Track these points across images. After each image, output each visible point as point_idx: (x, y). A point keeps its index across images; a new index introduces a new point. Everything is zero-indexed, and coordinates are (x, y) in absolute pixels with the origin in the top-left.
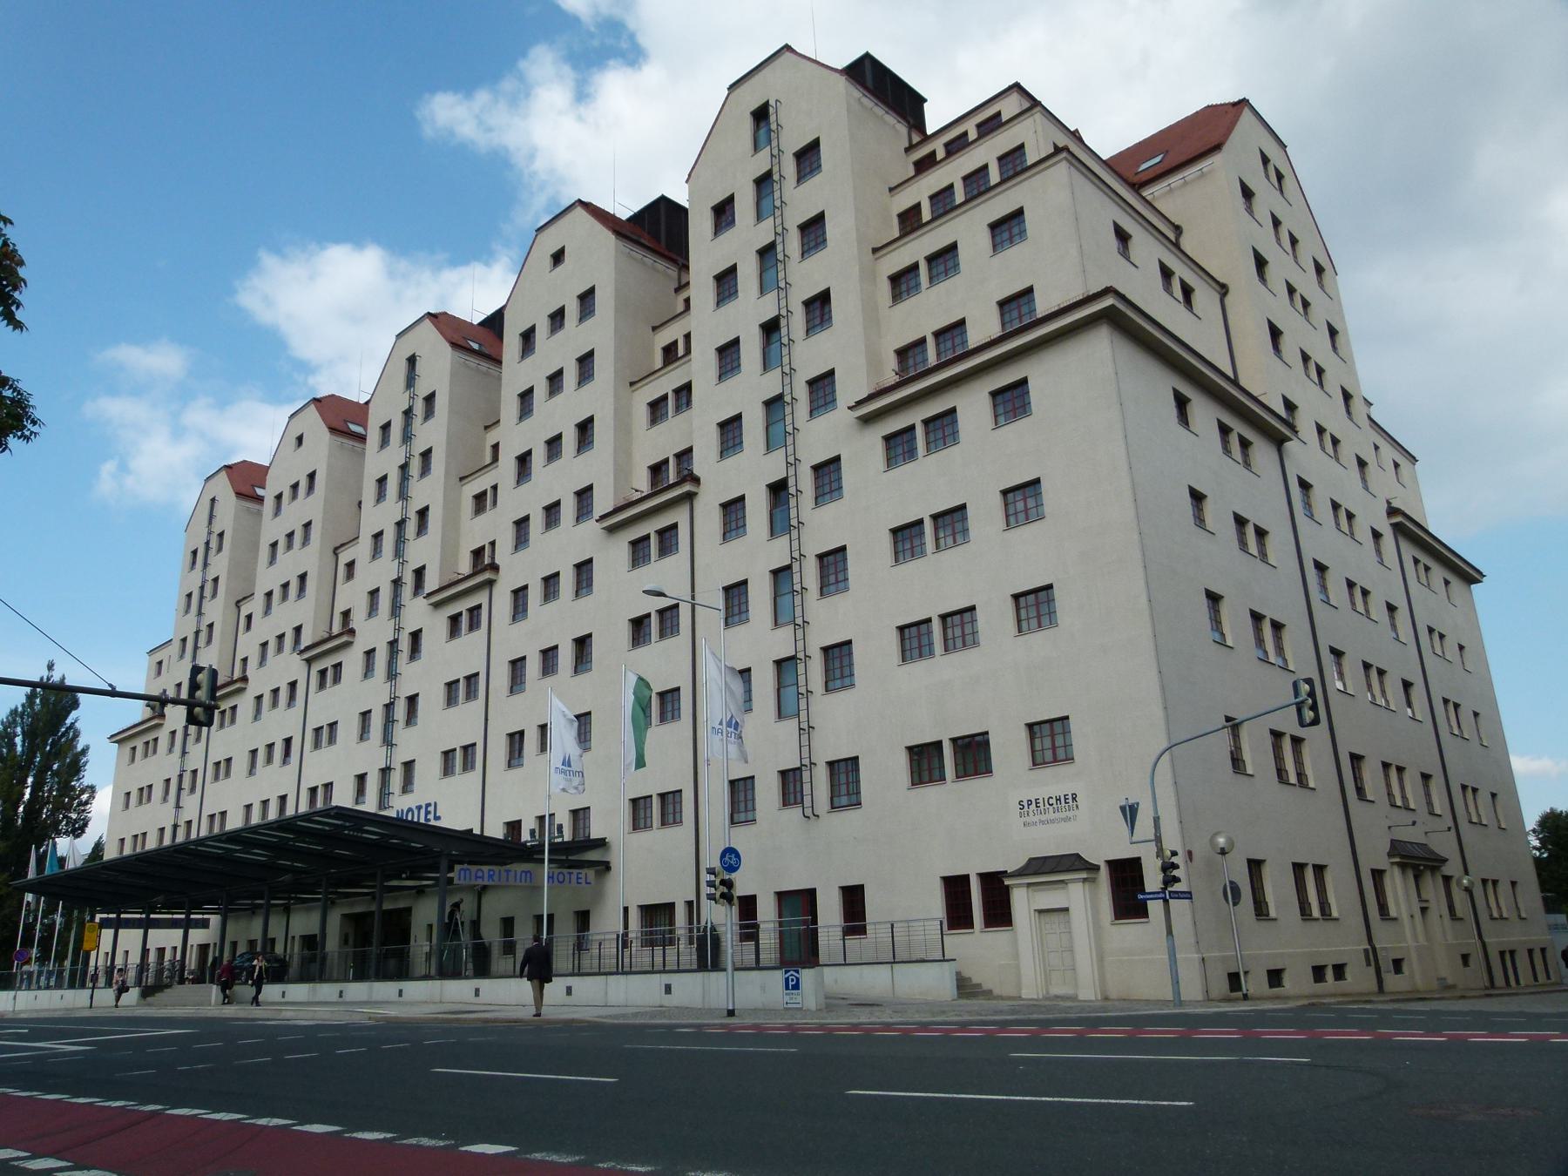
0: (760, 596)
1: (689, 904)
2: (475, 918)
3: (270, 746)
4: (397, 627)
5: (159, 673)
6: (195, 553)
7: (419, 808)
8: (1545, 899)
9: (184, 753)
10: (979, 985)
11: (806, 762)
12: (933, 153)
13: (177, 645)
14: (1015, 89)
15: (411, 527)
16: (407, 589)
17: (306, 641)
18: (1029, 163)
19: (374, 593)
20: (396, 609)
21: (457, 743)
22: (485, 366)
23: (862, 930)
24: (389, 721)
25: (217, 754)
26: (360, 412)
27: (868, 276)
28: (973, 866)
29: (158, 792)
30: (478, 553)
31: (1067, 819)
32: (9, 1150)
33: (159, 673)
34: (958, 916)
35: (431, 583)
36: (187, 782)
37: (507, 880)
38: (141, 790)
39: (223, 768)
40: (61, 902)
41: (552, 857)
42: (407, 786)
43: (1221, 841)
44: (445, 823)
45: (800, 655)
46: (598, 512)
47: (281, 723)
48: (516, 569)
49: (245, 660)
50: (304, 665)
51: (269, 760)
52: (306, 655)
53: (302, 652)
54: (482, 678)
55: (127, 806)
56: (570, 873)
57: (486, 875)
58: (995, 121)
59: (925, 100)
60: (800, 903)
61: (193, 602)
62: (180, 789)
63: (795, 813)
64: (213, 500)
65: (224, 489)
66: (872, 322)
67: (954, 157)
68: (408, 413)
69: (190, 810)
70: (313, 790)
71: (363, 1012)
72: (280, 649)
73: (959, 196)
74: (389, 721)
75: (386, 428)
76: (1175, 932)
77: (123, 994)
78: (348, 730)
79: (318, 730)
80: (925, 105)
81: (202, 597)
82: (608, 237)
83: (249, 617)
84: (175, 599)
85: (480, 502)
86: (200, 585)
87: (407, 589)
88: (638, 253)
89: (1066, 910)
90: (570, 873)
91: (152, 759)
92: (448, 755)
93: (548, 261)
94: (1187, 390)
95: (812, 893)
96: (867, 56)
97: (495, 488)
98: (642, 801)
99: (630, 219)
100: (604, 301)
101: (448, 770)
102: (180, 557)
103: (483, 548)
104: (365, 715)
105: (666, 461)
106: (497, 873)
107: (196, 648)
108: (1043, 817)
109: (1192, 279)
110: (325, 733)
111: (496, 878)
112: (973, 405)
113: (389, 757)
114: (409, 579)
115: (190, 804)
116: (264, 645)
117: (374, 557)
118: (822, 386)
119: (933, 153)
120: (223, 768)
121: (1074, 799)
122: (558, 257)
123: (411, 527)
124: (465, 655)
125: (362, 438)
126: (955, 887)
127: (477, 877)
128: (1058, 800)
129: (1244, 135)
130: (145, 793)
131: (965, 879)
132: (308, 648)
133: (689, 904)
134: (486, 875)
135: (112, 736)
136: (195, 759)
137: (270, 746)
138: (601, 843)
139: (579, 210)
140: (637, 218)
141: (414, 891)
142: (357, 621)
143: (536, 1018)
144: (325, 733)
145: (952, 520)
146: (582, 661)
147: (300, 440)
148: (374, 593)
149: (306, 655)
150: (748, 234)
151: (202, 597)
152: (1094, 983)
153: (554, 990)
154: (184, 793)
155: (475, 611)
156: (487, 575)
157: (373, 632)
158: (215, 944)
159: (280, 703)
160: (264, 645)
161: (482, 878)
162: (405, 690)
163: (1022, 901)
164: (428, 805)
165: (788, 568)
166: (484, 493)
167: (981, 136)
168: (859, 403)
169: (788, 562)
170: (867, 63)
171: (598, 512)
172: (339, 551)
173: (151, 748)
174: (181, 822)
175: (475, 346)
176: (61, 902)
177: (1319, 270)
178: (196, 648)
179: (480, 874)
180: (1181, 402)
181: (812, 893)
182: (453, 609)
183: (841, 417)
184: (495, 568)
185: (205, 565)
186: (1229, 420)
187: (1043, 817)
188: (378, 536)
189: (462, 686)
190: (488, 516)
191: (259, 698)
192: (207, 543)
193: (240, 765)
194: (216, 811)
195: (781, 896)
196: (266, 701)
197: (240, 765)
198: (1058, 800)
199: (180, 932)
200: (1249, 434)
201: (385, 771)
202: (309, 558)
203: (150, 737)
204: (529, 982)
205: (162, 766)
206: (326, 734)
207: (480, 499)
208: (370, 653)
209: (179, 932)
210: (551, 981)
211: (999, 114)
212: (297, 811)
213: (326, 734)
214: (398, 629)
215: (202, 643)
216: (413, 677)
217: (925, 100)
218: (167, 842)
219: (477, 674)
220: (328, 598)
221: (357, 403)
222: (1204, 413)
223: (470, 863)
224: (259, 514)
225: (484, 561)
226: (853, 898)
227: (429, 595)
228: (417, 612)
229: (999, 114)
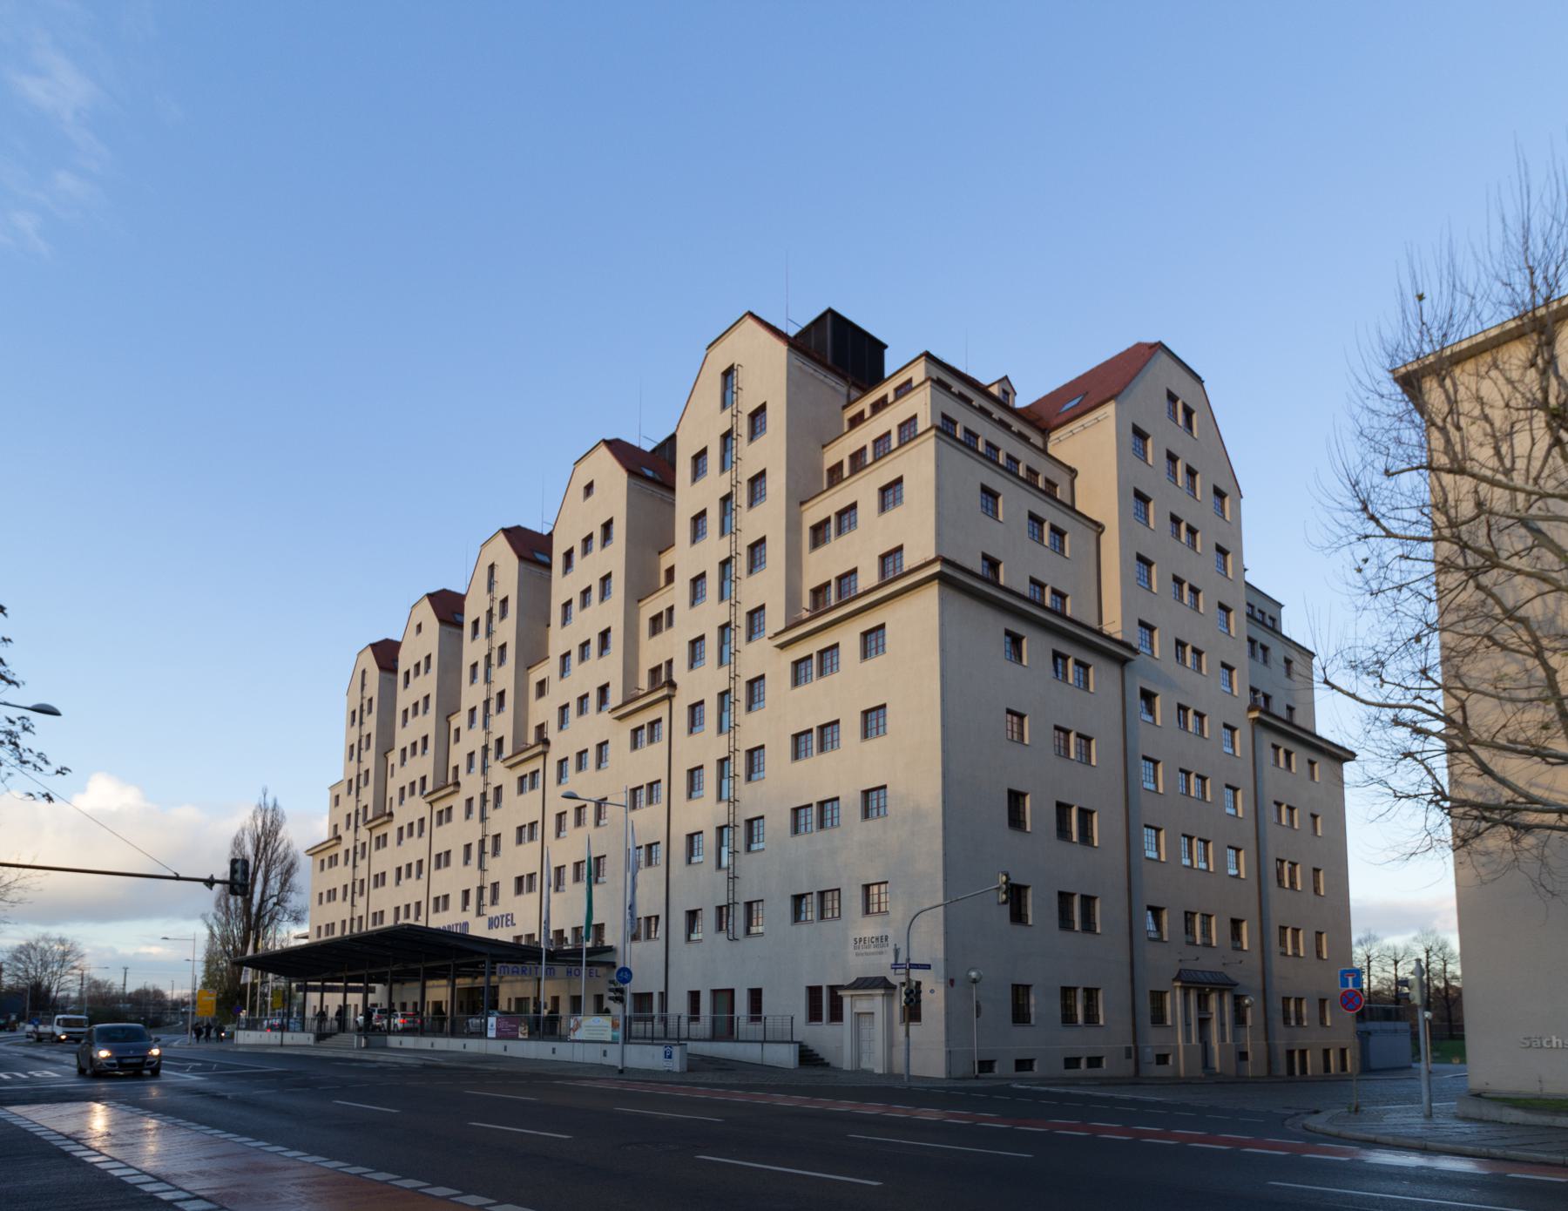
0: (710, 776)
1: (661, 993)
2: (663, 990)
4: (732, 675)
7: (502, 916)
8: (1463, 1030)
9: (355, 866)
10: (823, 1059)
11: (731, 901)
12: (886, 397)
13: (346, 785)
14: (923, 358)
15: (493, 705)
16: (492, 754)
17: (429, 788)
18: (919, 432)
19: (471, 755)
20: (484, 768)
21: (524, 872)
22: (659, 492)
23: (697, 1019)
24: (482, 852)
25: (376, 870)
26: (545, 542)
27: (793, 526)
28: (825, 982)
30: (655, 672)
31: (881, 953)
32: (383, 1174)
34: (814, 1015)
35: (508, 749)
36: (356, 889)
38: (329, 891)
39: (380, 879)
41: (589, 959)
42: (494, 899)
43: (973, 974)
44: (471, 932)
45: (731, 825)
46: (769, 631)
47: (414, 849)
48: (563, 744)
49: (456, 768)
50: (368, 832)
52: (429, 799)
53: (426, 796)
54: (664, 784)
55: (321, 902)
58: (908, 387)
59: (885, 347)
60: (724, 997)
61: (354, 752)
62: (353, 892)
63: (723, 936)
64: (492, 567)
67: (902, 400)
68: (490, 612)
69: (360, 910)
72: (412, 793)
73: (894, 443)
74: (482, 852)
75: (476, 623)
76: (911, 1035)
78: (457, 857)
79: (439, 856)
80: (887, 352)
81: (360, 749)
82: (781, 348)
83: (458, 730)
84: (342, 752)
85: (656, 624)
86: (486, 653)
87: (492, 754)
88: (810, 368)
89: (873, 1013)
91: (335, 869)
92: (519, 880)
93: (581, 492)
94: (1018, 628)
95: (732, 991)
96: (830, 311)
97: (671, 610)
98: (830, 894)
99: (654, 451)
100: (619, 531)
101: (519, 890)
102: (344, 718)
103: (660, 667)
104: (468, 847)
105: (828, 584)
107: (358, 788)
108: (868, 950)
109: (1063, 521)
110: (526, 831)
112: (848, 638)
113: (482, 879)
114: (492, 745)
115: (361, 902)
116: (564, 708)
117: (562, 676)
118: (756, 614)
119: (886, 397)
120: (380, 879)
121: (886, 940)
122: (589, 488)
123: (493, 705)
124: (648, 763)
125: (549, 566)
126: (814, 993)
128: (877, 939)
129: (1159, 375)
130: (332, 894)
131: (820, 988)
132: (430, 794)
133: (661, 993)
135: (308, 851)
136: (362, 873)
137: (409, 866)
138: (610, 949)
139: (749, 322)
140: (805, 332)
141: (69, 1009)
142: (552, 733)
144: (526, 831)
145: (827, 733)
146: (878, 733)
147: (419, 627)
148: (471, 755)
149: (429, 799)
150: (715, 484)
151: (360, 749)
155: (654, 724)
156: (665, 692)
157: (471, 785)
158: (447, 1002)
160: (564, 708)
162: (492, 832)
163: (851, 1005)
164: (508, 915)
165: (728, 759)
166: (660, 615)
167: (897, 398)
168: (777, 635)
169: (727, 755)
170: (829, 317)
171: (769, 631)
172: (451, 718)
173: (333, 860)
175: (649, 473)
177: (1219, 494)
178: (358, 788)
180: (1016, 640)
181: (732, 991)
182: (799, 651)
183: (763, 644)
184: (671, 684)
185: (361, 723)
186: (1064, 648)
187: (868, 950)
188: (473, 711)
189: (644, 792)
190: (665, 635)
191: (401, 829)
192: (362, 706)
193: (391, 878)
194: (378, 910)
195: (715, 992)
196: (571, 765)
197: (391, 878)
198: (877, 939)
199: (341, 995)
200: (1086, 657)
201: (481, 889)
202: (609, 613)
205: (340, 876)
206: (443, 859)
207: (656, 621)
208: (470, 801)
209: (341, 995)
211: (910, 381)
212: (396, 922)
213: (443, 859)
215: (362, 784)
216: (753, 728)
217: (885, 347)
218: (347, 932)
219: (536, 822)
220: (444, 756)
221: (541, 535)
222: (1036, 646)
223: (508, 962)
224: (460, 637)
225: (662, 678)
226: (756, 996)
227: (505, 760)
228: (500, 774)
229: (910, 381)
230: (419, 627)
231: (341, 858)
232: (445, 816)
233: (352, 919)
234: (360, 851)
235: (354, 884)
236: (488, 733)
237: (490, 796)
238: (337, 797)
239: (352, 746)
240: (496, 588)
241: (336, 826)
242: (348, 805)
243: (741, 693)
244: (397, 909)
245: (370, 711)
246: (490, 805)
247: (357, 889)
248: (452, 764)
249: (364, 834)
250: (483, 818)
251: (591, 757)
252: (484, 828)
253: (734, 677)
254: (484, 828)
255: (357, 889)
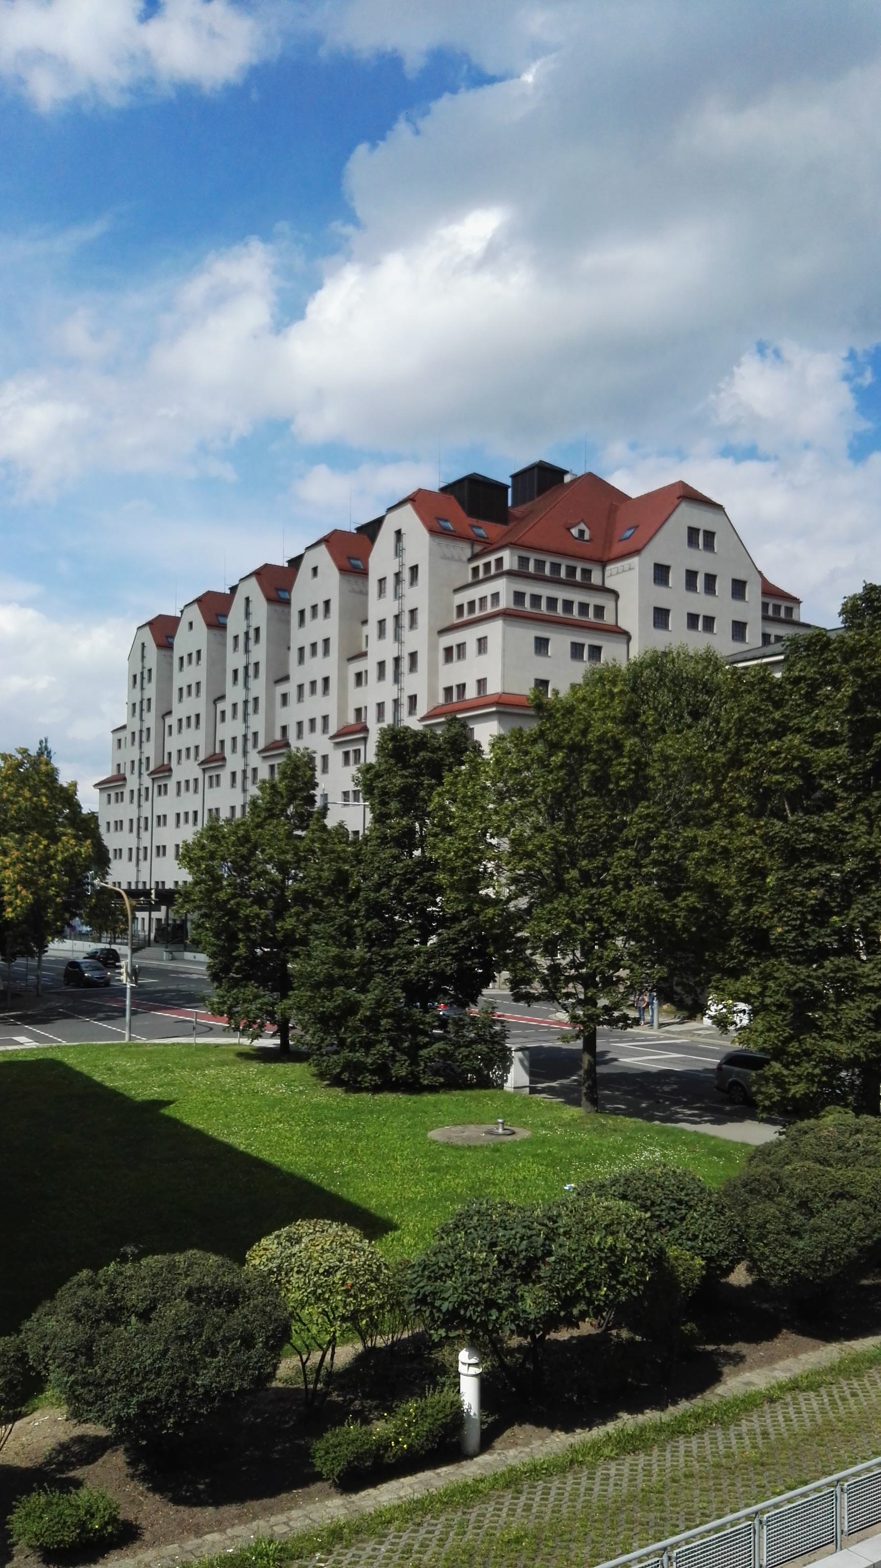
3: (190, 655)
5: (119, 746)
6: (135, 676)
9: (142, 688)
16: (250, 744)
25: (158, 811)
27: (433, 648)
29: (126, 825)
33: (119, 746)
39: (162, 820)
50: (201, 771)
51: (190, 662)
62: (142, 710)
65: (147, 636)
66: (433, 672)
70: (210, 810)
87: (250, 744)
93: (310, 573)
100: (334, 607)
113: (247, 695)
115: (145, 836)
120: (162, 820)
136: (146, 812)
137: (190, 655)
147: (191, 624)
154: (144, 713)
174: (144, 729)
203: (119, 791)
214: (249, 626)
220: (212, 731)
230: (191, 624)
231: (127, 796)
232: (215, 782)
233: (141, 731)
234: (143, 795)
235: (141, 702)
236: (247, 727)
237: (252, 634)
238: (119, 741)
239: (135, 676)
240: (252, 617)
241: (119, 765)
242: (132, 753)
243: (406, 575)
244: (178, 815)
245: (150, 680)
246: (252, 642)
247: (142, 824)
248: (219, 738)
249: (147, 782)
250: (247, 651)
251: (321, 609)
252: (248, 658)
253: (402, 565)
254: (248, 658)
255: (142, 824)
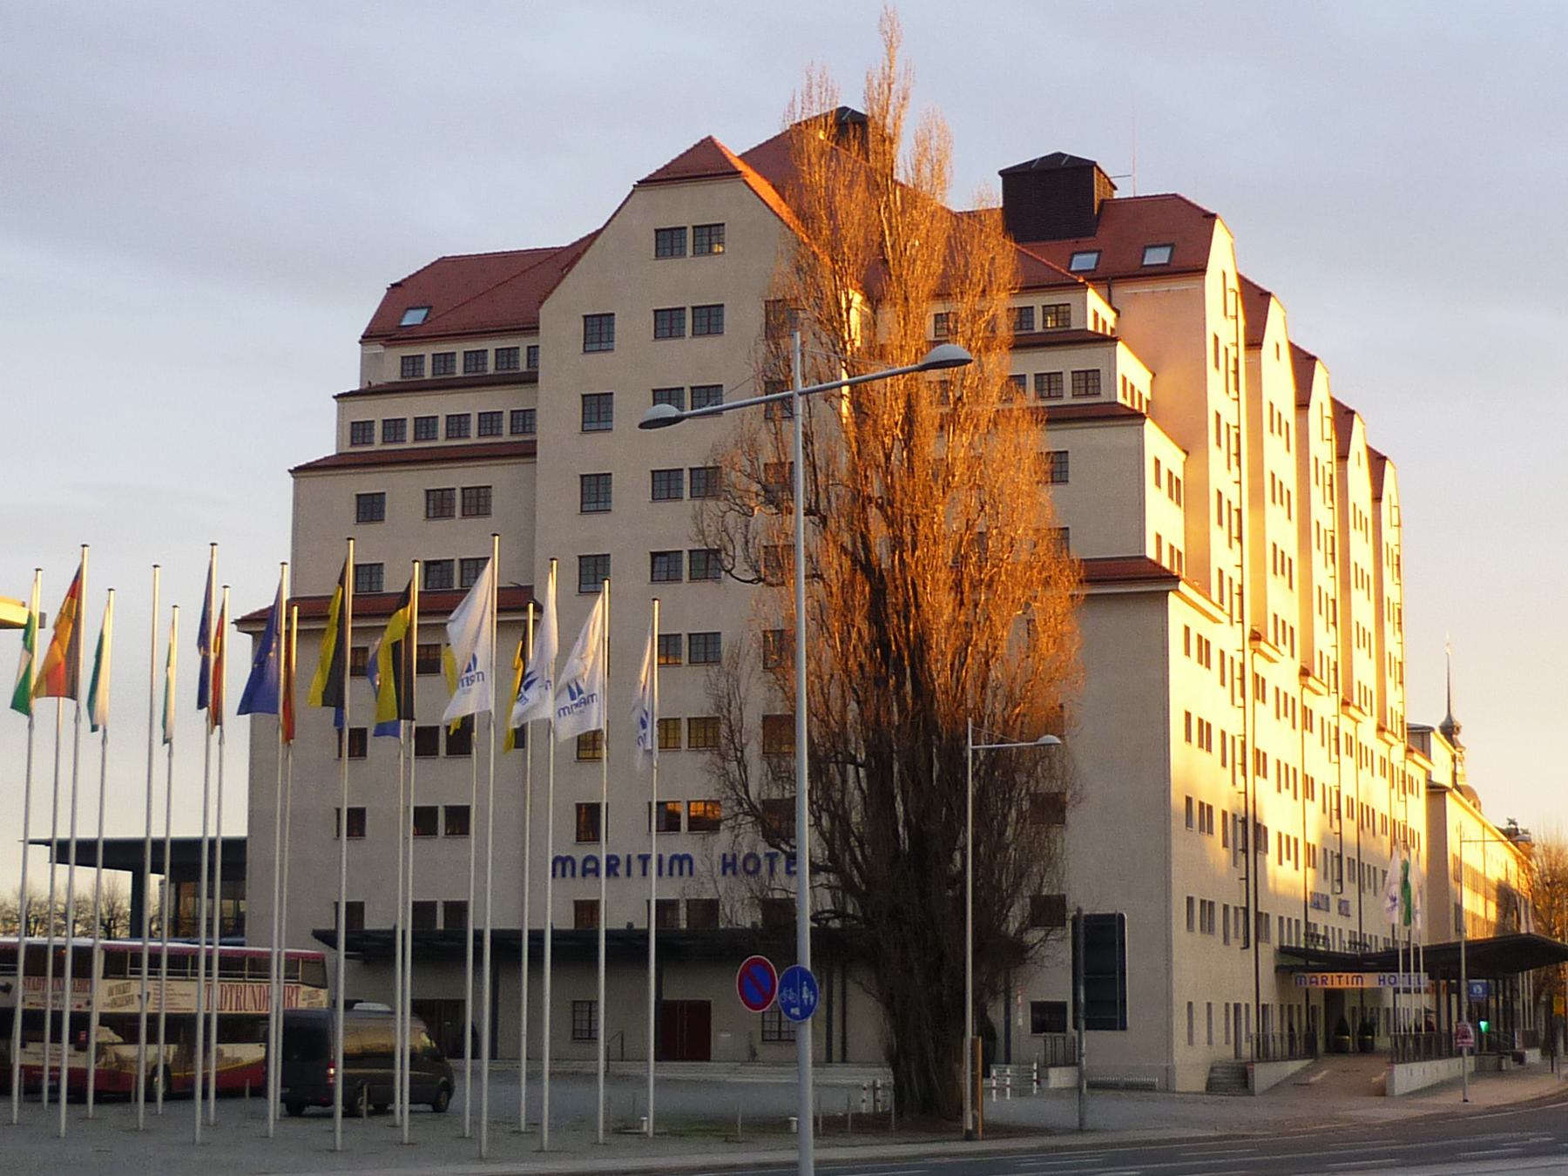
37: (1340, 983)
40: (440, 926)
56: (1340, 977)
57: (1320, 981)
71: (608, 758)
77: (272, 604)
90: (1340, 977)
106: (1330, 979)
111: (1329, 982)
127: (1311, 982)
131: (434, 810)
134: (1320, 981)
143: (1452, 906)
152: (491, 664)
153: (597, 692)
159: (664, 874)
161: (1317, 983)
176: (440, 926)
179: (1314, 979)
204: (1010, 244)
210: (1014, 178)
